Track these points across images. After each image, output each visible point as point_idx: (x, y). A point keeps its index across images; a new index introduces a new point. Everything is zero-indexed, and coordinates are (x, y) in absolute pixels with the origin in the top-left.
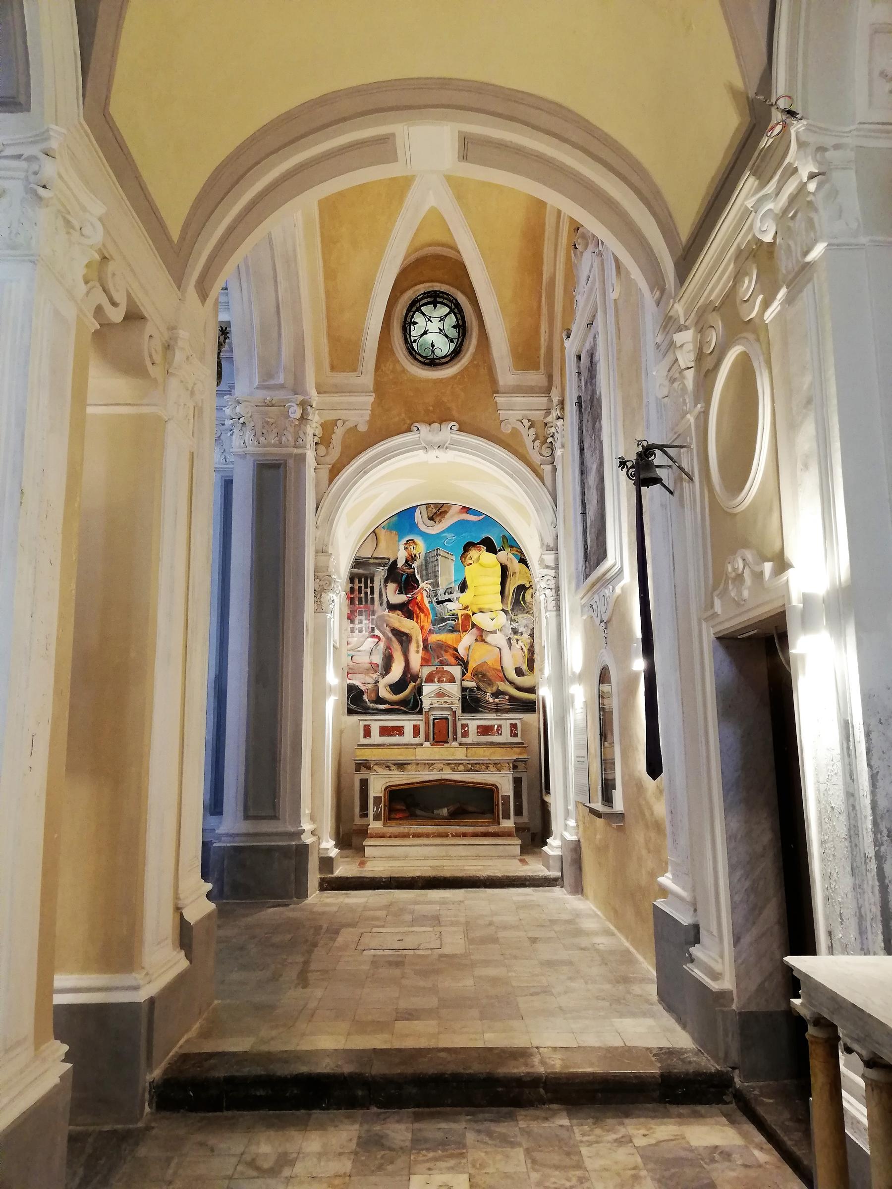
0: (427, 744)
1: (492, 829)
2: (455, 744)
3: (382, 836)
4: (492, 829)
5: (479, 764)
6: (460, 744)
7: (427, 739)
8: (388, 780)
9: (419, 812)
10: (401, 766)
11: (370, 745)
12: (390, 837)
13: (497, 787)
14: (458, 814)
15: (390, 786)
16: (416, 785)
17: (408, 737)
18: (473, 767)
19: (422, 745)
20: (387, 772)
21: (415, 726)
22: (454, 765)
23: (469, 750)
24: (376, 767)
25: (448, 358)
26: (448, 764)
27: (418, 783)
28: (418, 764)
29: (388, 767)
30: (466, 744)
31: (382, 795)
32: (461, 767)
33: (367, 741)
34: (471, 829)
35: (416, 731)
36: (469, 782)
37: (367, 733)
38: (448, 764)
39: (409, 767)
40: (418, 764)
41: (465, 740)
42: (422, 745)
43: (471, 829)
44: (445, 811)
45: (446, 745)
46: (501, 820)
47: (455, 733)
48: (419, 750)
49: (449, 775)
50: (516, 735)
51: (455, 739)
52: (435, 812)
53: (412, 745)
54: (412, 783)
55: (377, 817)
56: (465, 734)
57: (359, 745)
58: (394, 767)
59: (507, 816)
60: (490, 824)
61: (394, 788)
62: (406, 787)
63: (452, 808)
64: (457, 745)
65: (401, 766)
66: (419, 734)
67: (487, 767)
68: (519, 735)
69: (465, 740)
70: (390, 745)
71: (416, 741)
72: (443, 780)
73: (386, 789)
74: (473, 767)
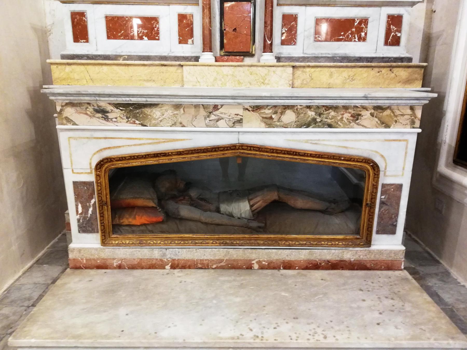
0: (208, 58)
1: (350, 254)
2: (268, 58)
3: (102, 266)
4: (350, 254)
5: (335, 108)
6: (278, 59)
7: (207, 46)
8: (104, 144)
9: (185, 211)
10: (135, 109)
11: (88, 57)
12: (120, 267)
13: (375, 167)
14: (271, 220)
15: (109, 160)
16: (175, 159)
17: (168, 41)
18: (320, 115)
19: (197, 59)
20: (97, 123)
21: (182, 17)
22: (270, 111)
23: (299, 72)
24: (69, 112)
25: (220, 149)
26: (256, 108)
27: (179, 153)
28: (177, 106)
29: (102, 112)
30: (291, 59)
31: (91, 178)
32: (289, 116)
33: (81, 48)
34: (302, 255)
35: (185, 29)
36: (305, 154)
37: (80, 31)
38: (256, 108)
39: (156, 113)
40: (177, 106)
41: (287, 51)
42: (197, 59)
43: (302, 255)
44: (242, 208)
45: (248, 61)
46: (375, 236)
47: (269, 34)
48: (189, 70)
49: (255, 133)
50: (396, 42)
51: (268, 48)
52: (224, 207)
53: (177, 58)
54: (165, 154)
55: (86, 227)
56: (290, 39)
57: (63, 57)
58: (116, 113)
59: (388, 228)
60: (348, 244)
61: (120, 164)
62: (151, 162)
63: (260, 201)
64: (274, 62)
65: (135, 109)
66: (191, 35)
67: (356, 117)
68: (403, 41)
69: (287, 51)
70: (130, 58)
71: (186, 50)
72: (242, 146)
73: (100, 165)
74: (320, 115)
